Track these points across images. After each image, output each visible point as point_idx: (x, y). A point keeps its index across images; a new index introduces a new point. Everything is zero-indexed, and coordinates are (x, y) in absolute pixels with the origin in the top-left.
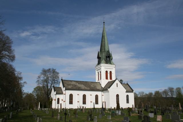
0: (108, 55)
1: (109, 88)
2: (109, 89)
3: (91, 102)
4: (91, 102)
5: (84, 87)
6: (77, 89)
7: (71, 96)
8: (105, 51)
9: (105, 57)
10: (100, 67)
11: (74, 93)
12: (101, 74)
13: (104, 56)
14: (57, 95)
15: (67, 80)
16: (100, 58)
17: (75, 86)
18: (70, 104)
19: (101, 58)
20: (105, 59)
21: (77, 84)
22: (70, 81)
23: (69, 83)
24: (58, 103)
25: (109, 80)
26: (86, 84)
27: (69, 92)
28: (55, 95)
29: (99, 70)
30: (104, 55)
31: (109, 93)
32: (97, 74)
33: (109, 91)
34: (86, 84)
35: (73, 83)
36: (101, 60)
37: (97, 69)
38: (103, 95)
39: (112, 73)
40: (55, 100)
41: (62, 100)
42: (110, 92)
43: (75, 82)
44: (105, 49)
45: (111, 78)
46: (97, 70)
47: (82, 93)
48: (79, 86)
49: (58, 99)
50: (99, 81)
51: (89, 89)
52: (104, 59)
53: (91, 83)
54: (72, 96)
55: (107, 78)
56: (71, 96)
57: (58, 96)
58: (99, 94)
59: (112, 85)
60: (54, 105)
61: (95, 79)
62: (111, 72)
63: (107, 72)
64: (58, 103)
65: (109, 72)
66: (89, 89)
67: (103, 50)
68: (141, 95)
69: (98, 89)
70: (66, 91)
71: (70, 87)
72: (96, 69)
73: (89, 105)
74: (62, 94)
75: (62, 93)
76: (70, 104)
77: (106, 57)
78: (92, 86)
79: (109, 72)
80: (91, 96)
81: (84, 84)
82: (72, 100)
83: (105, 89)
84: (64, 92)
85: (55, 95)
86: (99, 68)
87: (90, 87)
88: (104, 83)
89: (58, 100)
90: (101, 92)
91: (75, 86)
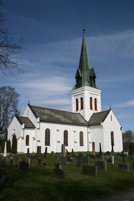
0: (93, 76)
1: (103, 121)
3: (59, 142)
4: (59, 142)
5: (64, 118)
6: (56, 121)
7: (48, 132)
8: (87, 69)
9: (89, 78)
11: (53, 127)
13: (85, 75)
14: (25, 130)
15: (36, 107)
17: (52, 116)
18: (41, 147)
19: (83, 78)
20: (89, 80)
21: (53, 114)
22: (41, 108)
23: (42, 112)
25: (94, 111)
26: (64, 115)
27: (45, 126)
28: (22, 129)
29: (78, 96)
30: (86, 74)
31: (104, 129)
32: (74, 101)
33: (102, 126)
34: (64, 115)
35: (47, 112)
36: (83, 81)
37: (74, 95)
38: (89, 133)
39: (97, 101)
41: (34, 139)
43: (48, 111)
44: (87, 66)
45: (96, 109)
46: (74, 96)
47: (63, 128)
48: (60, 117)
49: (28, 137)
50: (80, 111)
51: (70, 122)
52: (87, 80)
53: (69, 113)
55: (91, 108)
56: (48, 132)
57: (28, 132)
58: (84, 129)
59: (30, 120)
60: (22, 148)
61: (70, 105)
62: (95, 99)
63: (91, 98)
64: (27, 143)
66: (70, 122)
67: (85, 68)
68: (39, 148)
69: (81, 123)
71: (45, 117)
72: (73, 94)
73: (55, 147)
74: (34, 128)
76: (41, 147)
77: (90, 77)
78: (75, 120)
79: (93, 100)
81: (62, 115)
83: (93, 124)
85: (22, 129)
87: (70, 118)
88: (88, 114)
91: (52, 116)
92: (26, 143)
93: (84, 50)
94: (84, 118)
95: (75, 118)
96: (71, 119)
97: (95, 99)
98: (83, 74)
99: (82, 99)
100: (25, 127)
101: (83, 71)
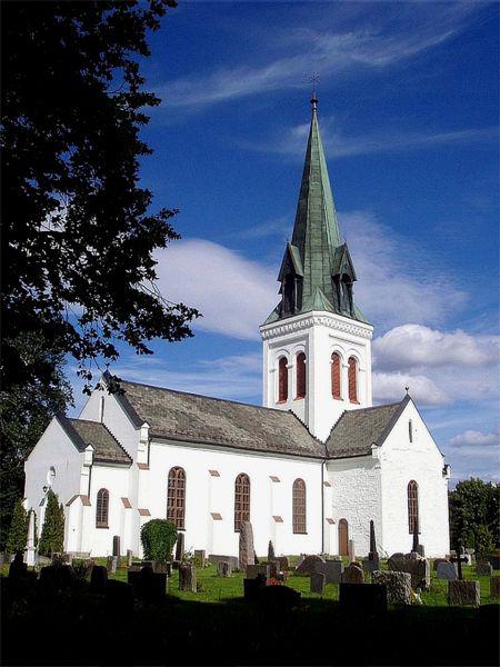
1: (379, 443)
2: (378, 452)
8: (324, 247)
9: (328, 281)
10: (304, 328)
12: (214, 382)
16: (302, 278)
20: (329, 289)
21: (195, 411)
24: (102, 519)
27: (167, 456)
30: (320, 265)
36: (306, 289)
37: (271, 341)
40: (86, 501)
41: (126, 503)
42: (383, 464)
43: (179, 400)
44: (324, 237)
47: (232, 464)
49: (103, 497)
54: (248, 488)
55: (336, 393)
57: (105, 477)
58: (310, 471)
62: (352, 360)
63: (336, 356)
64: (102, 519)
65: (293, 362)
67: (316, 242)
70: (153, 445)
71: (167, 424)
72: (267, 338)
75: (124, 460)
79: (344, 361)
80: (272, 477)
82: (183, 505)
84: (141, 458)
86: (295, 330)
87: (256, 429)
88: (324, 413)
89: (99, 501)
90: (318, 467)
91: (192, 420)
92: (98, 520)
93: (311, 177)
94: (310, 427)
95: (275, 427)
96: (263, 434)
97: (352, 360)
98: (307, 263)
99: (302, 357)
100: (95, 460)
101: (306, 254)
